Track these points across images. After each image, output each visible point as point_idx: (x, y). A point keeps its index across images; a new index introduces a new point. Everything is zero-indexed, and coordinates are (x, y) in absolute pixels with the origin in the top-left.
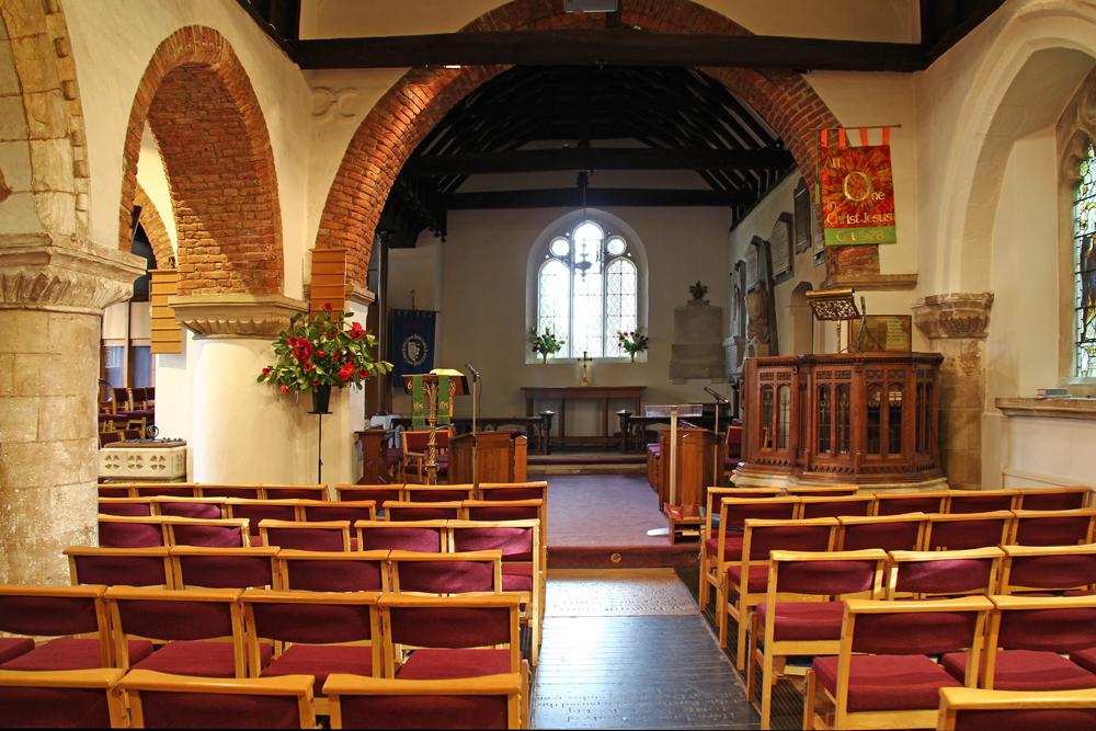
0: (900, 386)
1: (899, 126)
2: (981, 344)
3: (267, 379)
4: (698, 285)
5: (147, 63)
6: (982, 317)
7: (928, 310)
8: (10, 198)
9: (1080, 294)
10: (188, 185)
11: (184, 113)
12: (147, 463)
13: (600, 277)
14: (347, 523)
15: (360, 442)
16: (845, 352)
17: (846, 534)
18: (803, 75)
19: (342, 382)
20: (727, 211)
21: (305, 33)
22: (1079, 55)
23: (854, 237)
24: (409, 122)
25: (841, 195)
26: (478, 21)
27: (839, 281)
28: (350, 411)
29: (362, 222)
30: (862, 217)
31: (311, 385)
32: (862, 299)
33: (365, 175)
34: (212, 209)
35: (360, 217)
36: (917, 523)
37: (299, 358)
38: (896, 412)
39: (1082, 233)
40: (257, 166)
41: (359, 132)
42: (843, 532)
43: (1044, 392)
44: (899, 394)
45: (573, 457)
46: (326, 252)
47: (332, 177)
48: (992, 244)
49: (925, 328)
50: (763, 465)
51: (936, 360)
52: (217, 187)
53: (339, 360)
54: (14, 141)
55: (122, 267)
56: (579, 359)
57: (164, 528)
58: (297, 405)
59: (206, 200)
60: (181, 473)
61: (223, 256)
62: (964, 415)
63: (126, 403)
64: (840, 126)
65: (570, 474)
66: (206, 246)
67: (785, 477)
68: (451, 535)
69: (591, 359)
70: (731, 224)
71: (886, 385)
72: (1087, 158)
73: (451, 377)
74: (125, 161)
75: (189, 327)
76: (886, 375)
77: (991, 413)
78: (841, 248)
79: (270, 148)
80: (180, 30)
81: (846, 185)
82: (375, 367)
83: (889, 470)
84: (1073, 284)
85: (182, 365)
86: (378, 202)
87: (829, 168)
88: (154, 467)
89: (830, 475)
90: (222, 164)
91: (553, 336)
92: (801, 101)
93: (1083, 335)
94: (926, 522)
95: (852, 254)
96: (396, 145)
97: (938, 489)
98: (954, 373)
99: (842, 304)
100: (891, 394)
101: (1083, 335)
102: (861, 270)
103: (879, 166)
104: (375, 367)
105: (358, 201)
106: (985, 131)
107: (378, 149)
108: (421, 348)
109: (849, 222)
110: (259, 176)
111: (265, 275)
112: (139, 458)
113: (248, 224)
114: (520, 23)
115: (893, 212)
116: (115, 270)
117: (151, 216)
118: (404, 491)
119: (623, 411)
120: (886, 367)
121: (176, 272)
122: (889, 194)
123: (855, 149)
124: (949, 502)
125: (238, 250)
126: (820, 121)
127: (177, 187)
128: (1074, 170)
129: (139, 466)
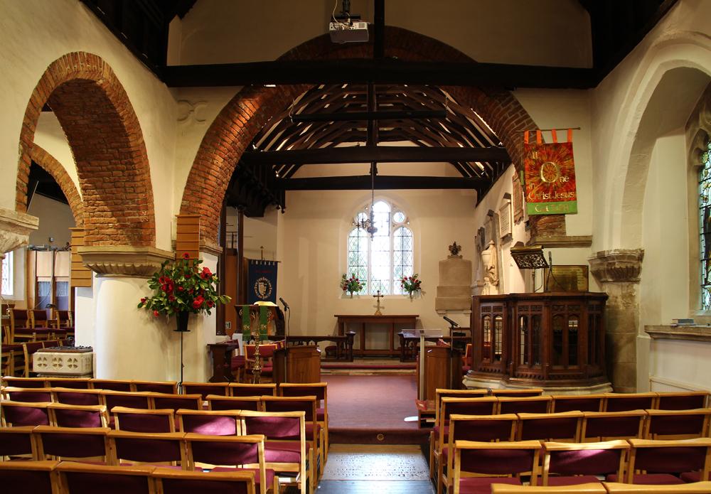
0: (576, 316)
1: (579, 129)
2: (635, 286)
3: (144, 306)
4: (455, 244)
5: (40, 77)
6: (636, 266)
7: (599, 262)
9: (703, 250)
10: (89, 168)
11: (83, 116)
12: (65, 363)
13: (388, 239)
14: (171, 411)
15: (212, 353)
16: (541, 291)
17: (523, 425)
18: (511, 91)
19: (196, 310)
20: (474, 192)
21: (173, 59)
22: (696, 74)
23: (548, 209)
24: (242, 125)
25: (539, 178)
26: (288, 53)
27: (537, 240)
28: (206, 330)
29: (211, 196)
30: (553, 194)
31: (174, 311)
32: (550, 253)
33: (213, 163)
34: (105, 185)
35: (210, 193)
36: (575, 419)
37: (166, 292)
38: (573, 334)
39: (704, 205)
40: (134, 155)
41: (208, 133)
42: (521, 425)
43: (677, 322)
44: (576, 322)
45: (368, 363)
46: (187, 217)
47: (191, 164)
48: (643, 214)
49: (597, 275)
50: (484, 372)
51: (603, 298)
52: (109, 170)
53: (194, 294)
55: (17, 223)
56: (374, 296)
57: (49, 412)
58: (168, 325)
59: (101, 179)
60: (88, 371)
61: (114, 219)
62: (624, 337)
63: (28, 322)
64: (538, 129)
65: (366, 376)
66: (102, 211)
67: (498, 381)
68: (243, 421)
69: (382, 296)
71: (566, 316)
72: (707, 150)
73: (269, 307)
74: (22, 148)
75: (92, 268)
76: (566, 309)
77: (642, 336)
78: (539, 217)
79: (143, 142)
80: (68, 55)
81: (542, 172)
82: (219, 298)
83: (568, 377)
84: (699, 241)
85: (91, 296)
86: (224, 183)
87: (530, 159)
88: (70, 366)
89: (528, 380)
90: (111, 153)
91: (357, 280)
92: (510, 111)
93: (706, 279)
94: (583, 418)
95: (547, 222)
96: (233, 142)
97: (605, 392)
98: (617, 307)
99: (535, 257)
100: (570, 322)
101: (706, 279)
102: (553, 233)
103: (565, 157)
104: (219, 298)
105: (208, 181)
106: (636, 131)
107: (221, 144)
109: (544, 198)
110: (135, 162)
111: (141, 231)
112: (60, 359)
113: (130, 196)
114: (317, 55)
115: (575, 190)
116: (12, 226)
117: (72, 190)
118: (229, 387)
120: (567, 303)
121: (83, 230)
122: (572, 178)
123: (548, 145)
124: (606, 402)
125: (124, 215)
126: (524, 125)
127: (82, 169)
128: (699, 159)
129: (60, 365)
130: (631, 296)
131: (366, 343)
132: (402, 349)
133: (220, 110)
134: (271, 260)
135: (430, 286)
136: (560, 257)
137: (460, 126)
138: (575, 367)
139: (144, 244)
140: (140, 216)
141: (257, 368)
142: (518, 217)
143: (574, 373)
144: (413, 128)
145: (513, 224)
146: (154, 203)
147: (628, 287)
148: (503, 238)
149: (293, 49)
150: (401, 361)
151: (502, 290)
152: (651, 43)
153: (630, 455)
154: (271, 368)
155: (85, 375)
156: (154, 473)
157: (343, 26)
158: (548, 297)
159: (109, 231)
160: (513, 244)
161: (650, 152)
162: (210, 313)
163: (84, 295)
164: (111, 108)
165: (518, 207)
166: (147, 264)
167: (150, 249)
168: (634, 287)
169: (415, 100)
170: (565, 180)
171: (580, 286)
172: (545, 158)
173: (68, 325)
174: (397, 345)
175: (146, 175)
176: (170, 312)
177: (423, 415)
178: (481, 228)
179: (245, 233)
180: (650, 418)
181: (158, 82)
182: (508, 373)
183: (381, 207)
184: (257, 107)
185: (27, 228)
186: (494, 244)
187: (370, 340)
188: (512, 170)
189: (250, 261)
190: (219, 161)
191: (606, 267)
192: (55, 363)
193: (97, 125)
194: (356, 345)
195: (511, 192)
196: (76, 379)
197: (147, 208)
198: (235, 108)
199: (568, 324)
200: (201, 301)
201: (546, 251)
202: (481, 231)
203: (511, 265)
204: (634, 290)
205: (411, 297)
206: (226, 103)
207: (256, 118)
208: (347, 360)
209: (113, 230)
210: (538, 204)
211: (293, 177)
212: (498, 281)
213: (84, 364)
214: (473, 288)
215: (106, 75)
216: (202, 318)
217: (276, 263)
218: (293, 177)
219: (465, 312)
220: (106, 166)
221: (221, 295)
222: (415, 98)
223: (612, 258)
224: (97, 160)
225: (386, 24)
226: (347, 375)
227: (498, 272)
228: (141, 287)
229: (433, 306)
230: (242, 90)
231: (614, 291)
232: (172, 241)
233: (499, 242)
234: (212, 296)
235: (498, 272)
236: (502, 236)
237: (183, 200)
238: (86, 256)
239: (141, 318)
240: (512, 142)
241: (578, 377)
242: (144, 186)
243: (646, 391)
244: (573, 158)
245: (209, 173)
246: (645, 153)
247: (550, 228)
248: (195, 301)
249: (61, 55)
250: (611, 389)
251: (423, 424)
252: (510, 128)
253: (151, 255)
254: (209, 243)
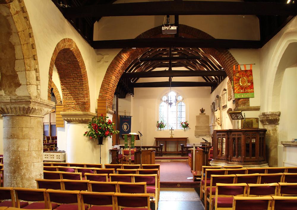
0: (255, 138)
1: (255, 64)
2: (277, 126)
3: (86, 135)
4: (202, 109)
6: (278, 118)
7: (263, 116)
10: (65, 81)
11: (64, 62)
12: (55, 157)
15: (111, 152)
16: (241, 128)
18: (228, 50)
19: (106, 136)
20: (210, 88)
21: (95, 39)
23: (243, 96)
26: (140, 35)
28: (109, 144)
30: (245, 90)
31: (98, 137)
32: (244, 114)
33: (111, 79)
35: (110, 90)
36: (257, 176)
37: (94, 129)
38: (254, 145)
40: (83, 76)
44: (254, 140)
45: (169, 157)
46: (102, 99)
47: (103, 79)
49: (262, 122)
50: (218, 160)
51: (265, 131)
52: (73, 82)
53: (105, 130)
54: (22, 71)
56: (170, 130)
59: (70, 86)
60: (64, 160)
61: (74, 101)
64: (239, 64)
65: (294, 147)
66: (70, 98)
69: (173, 130)
70: (211, 92)
71: (251, 138)
75: (66, 120)
77: (280, 146)
78: (239, 99)
79: (86, 71)
81: (240, 81)
82: (115, 132)
83: (252, 161)
85: (64, 131)
87: (236, 76)
88: (57, 158)
89: (236, 163)
91: (163, 123)
94: (260, 176)
95: (242, 101)
97: (266, 167)
98: (270, 134)
100: (252, 140)
102: (244, 105)
103: (249, 75)
106: (277, 66)
107: (115, 71)
108: (127, 126)
111: (85, 106)
113: (81, 92)
115: (253, 88)
119: (182, 145)
120: (251, 133)
122: (252, 83)
124: (267, 170)
126: (233, 63)
130: (276, 130)
131: (167, 149)
132: (182, 151)
133: (114, 58)
134: (129, 115)
135: (193, 125)
136: (248, 115)
137: (205, 62)
138: (254, 158)
139: (86, 111)
140: (85, 100)
141: (130, 158)
142: (230, 99)
143: (253, 160)
144: (185, 62)
145: (227, 101)
146: (90, 95)
147: (274, 126)
148: (223, 107)
149: (143, 34)
150: (182, 156)
151: (222, 127)
152: (284, 32)
153: (279, 189)
154: (134, 159)
155: (62, 162)
157: (167, 28)
158: (244, 131)
159: (72, 106)
160: (228, 109)
161: (283, 74)
162: (111, 137)
163: (61, 131)
165: (230, 94)
167: (89, 113)
168: (277, 127)
169: (186, 51)
170: (249, 84)
171: (255, 126)
172: (241, 76)
173: (50, 142)
174: (180, 149)
175: (87, 84)
176: (96, 137)
177: (195, 177)
178: (213, 102)
179: (119, 105)
180: (285, 176)
181: (90, 47)
182: (228, 159)
183: (172, 93)
184: (128, 56)
185: (51, 106)
186: (219, 109)
187: (168, 148)
188: (227, 79)
189: (120, 116)
190: (114, 78)
191: (266, 118)
192: (51, 157)
193: (69, 65)
194: (163, 150)
195: (226, 88)
197: (87, 97)
198: (120, 57)
199: (252, 141)
200: (108, 133)
201: (243, 113)
202: (213, 103)
203: (227, 118)
204: (277, 128)
205: (185, 130)
206: (116, 55)
207: (128, 60)
208: (160, 156)
209: (74, 105)
210: (239, 94)
211: (136, 82)
212: (221, 124)
213: (63, 157)
214: (210, 126)
215: (74, 46)
216: (108, 139)
217: (131, 117)
218: (136, 82)
219: (207, 136)
220: (72, 80)
222: (187, 50)
223: (269, 115)
224: (69, 78)
225: (179, 23)
226: (160, 161)
227: (221, 120)
228: (85, 127)
229: (193, 133)
231: (269, 128)
233: (221, 108)
234: (112, 131)
235: (221, 120)
236: (222, 106)
237: (100, 93)
238: (64, 115)
239: (85, 140)
240: (229, 70)
241: (256, 161)
242: (86, 88)
243: (282, 167)
244: (252, 75)
245: (110, 83)
246: (281, 74)
247: (244, 103)
248: (106, 133)
249: (60, 40)
250: (268, 166)
251: (195, 180)
252: (228, 64)
253: (89, 115)
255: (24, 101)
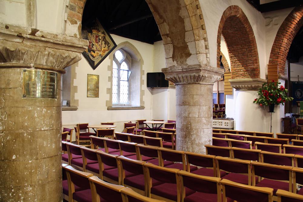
3: (256, 102)
5: (221, 18)
8: (191, 56)
11: (231, 29)
12: (224, 124)
14: (280, 145)
19: (278, 103)
24: (296, 24)
28: (280, 112)
29: (282, 56)
33: (283, 42)
34: (240, 55)
35: (282, 54)
40: (251, 42)
41: (280, 29)
46: (272, 65)
47: (273, 43)
52: (240, 49)
53: (277, 97)
54: (191, 42)
55: (218, 72)
57: (229, 142)
58: (264, 109)
60: (232, 127)
61: (243, 68)
79: (254, 36)
82: (288, 99)
85: (233, 98)
86: (287, 49)
88: (225, 125)
96: (292, 31)
105: (281, 49)
107: (286, 33)
110: (252, 45)
111: (254, 72)
112: (222, 123)
116: (216, 73)
125: (247, 66)
129: (222, 125)
133: (285, 19)
155: (231, 129)
156: (90, 178)
163: (230, 98)
164: (242, 25)
166: (258, 85)
167: (258, 79)
193: (236, 32)
196: (229, 130)
209: (242, 72)
213: (231, 125)
216: (280, 106)
221: (289, 97)
230: (295, 8)
232: (266, 75)
237: (270, 58)
238: (232, 83)
242: (255, 54)
254: (282, 76)
255: (195, 69)
